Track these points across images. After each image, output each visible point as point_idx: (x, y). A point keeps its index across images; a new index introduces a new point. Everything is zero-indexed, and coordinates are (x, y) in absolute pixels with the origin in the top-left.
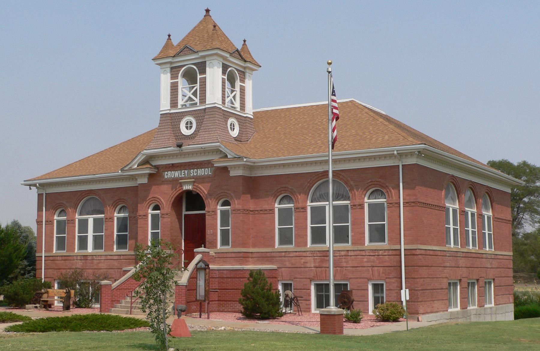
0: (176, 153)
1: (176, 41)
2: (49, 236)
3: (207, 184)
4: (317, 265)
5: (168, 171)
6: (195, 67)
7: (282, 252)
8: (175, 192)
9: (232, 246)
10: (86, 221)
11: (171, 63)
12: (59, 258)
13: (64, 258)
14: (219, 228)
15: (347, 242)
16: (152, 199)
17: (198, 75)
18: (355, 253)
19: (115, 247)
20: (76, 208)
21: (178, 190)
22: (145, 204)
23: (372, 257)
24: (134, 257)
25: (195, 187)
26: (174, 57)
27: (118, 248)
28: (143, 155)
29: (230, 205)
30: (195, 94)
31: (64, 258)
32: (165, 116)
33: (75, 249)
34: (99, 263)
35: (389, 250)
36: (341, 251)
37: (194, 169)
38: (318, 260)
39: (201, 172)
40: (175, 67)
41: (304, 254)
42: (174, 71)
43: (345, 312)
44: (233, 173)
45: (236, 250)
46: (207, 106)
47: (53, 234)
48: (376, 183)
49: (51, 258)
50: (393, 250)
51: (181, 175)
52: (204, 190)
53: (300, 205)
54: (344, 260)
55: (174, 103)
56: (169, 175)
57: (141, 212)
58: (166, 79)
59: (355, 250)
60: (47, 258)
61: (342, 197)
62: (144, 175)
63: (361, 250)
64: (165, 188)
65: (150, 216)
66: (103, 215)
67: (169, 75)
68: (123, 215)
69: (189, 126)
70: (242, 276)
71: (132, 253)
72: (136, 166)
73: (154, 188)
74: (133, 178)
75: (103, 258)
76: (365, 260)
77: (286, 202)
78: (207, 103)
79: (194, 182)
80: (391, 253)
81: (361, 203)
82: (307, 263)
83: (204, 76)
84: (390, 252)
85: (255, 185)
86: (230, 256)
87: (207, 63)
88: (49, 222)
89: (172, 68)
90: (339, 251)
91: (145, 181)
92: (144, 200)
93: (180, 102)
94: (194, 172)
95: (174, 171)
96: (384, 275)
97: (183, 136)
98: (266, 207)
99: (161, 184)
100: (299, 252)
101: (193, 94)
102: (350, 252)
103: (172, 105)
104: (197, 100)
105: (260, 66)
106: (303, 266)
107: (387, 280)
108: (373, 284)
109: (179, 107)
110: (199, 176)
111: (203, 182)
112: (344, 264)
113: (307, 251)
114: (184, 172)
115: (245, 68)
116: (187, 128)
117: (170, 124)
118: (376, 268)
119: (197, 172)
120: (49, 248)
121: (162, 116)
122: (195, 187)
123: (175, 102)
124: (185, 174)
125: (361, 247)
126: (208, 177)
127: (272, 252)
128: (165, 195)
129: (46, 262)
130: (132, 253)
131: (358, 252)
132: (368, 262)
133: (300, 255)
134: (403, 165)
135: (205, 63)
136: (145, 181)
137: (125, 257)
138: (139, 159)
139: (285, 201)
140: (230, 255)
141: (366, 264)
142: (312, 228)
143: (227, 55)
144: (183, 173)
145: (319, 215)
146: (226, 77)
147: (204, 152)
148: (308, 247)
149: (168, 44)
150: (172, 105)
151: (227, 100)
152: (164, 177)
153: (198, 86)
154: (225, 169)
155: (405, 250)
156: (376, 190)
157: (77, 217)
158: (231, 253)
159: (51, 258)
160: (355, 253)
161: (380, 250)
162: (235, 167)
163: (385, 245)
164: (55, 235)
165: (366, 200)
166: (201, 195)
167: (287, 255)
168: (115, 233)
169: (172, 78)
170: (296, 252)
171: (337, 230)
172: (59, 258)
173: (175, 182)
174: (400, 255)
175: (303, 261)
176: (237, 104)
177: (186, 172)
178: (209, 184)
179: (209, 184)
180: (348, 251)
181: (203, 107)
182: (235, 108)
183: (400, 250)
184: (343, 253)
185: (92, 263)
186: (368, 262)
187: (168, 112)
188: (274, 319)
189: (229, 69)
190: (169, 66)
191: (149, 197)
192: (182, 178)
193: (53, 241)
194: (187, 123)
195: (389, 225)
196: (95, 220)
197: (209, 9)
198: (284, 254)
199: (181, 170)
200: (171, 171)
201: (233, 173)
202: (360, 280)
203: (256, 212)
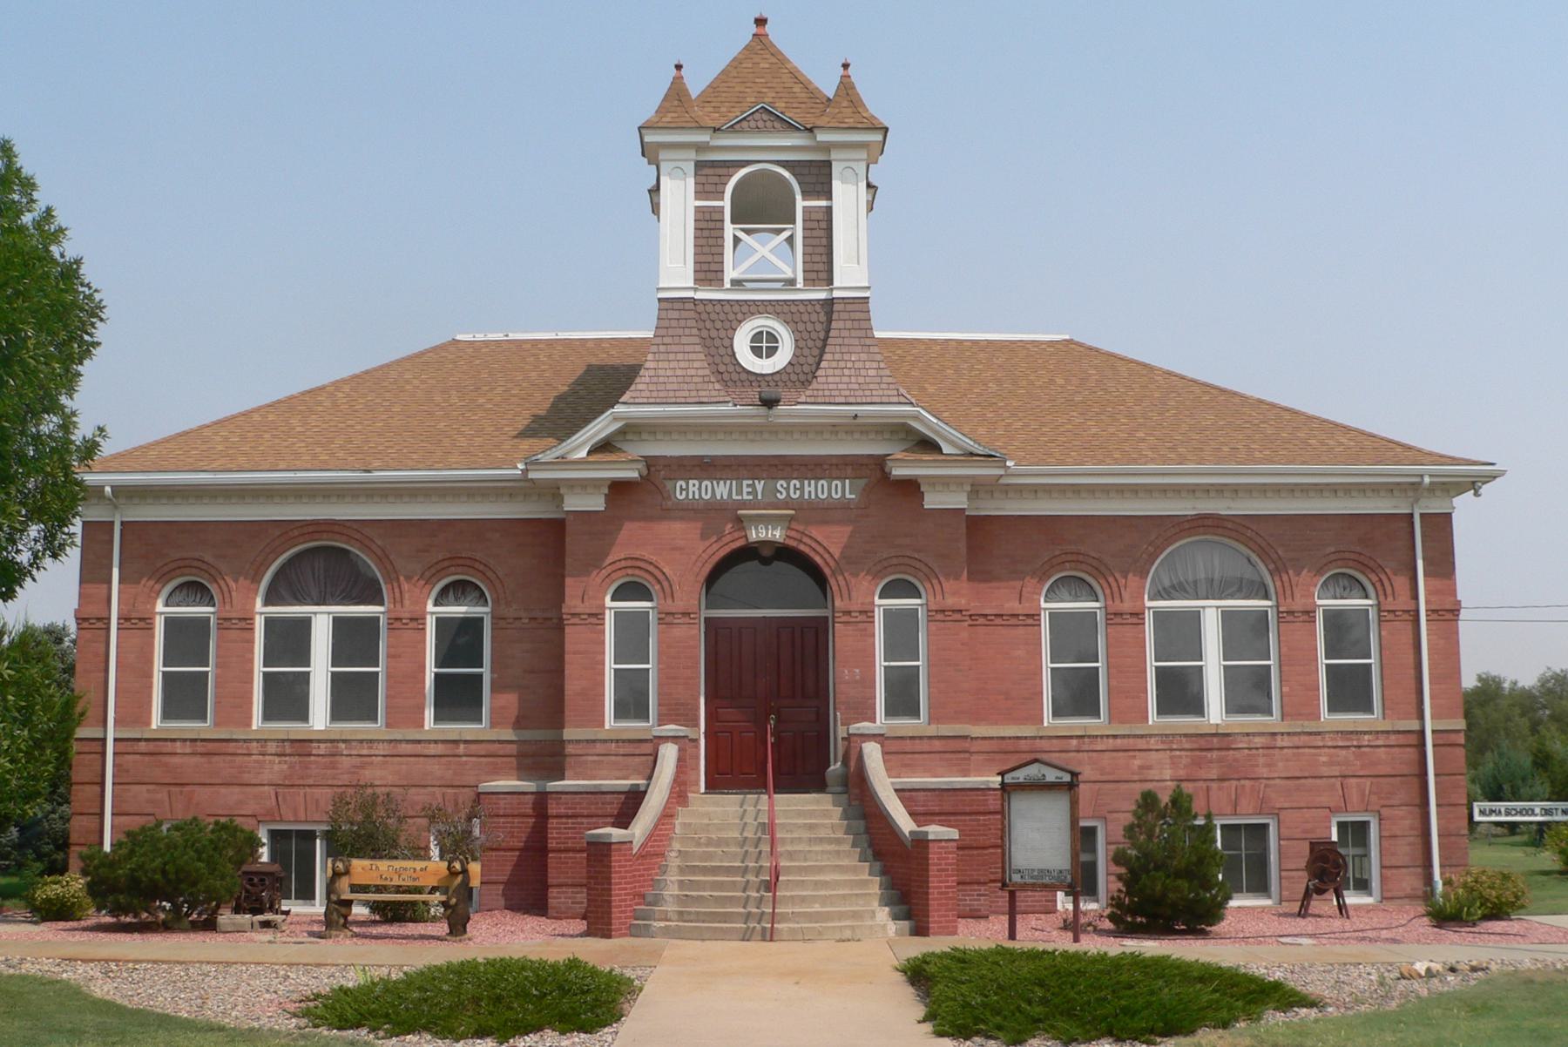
0: (757, 425)
1: (696, 85)
2: (137, 669)
3: (836, 528)
4: (1182, 773)
5: (687, 480)
6: (786, 174)
7: (1071, 737)
8: (715, 547)
9: (1111, 719)
10: (304, 625)
11: (700, 147)
12: (178, 747)
13: (200, 747)
14: (610, 666)
15: (373, 718)
16: (623, 564)
17: (799, 197)
18: (1296, 741)
19: (429, 713)
20: (256, 579)
21: (725, 540)
22: (596, 578)
23: (1344, 752)
24: (513, 749)
25: (793, 534)
26: (716, 130)
27: (438, 718)
28: (616, 419)
29: (651, 600)
31: (200, 747)
32: (677, 306)
33: (250, 718)
34: (362, 767)
35: (1388, 732)
36: (1254, 734)
37: (788, 479)
38: (1184, 761)
39: (816, 490)
40: (714, 164)
41: (1141, 744)
42: (709, 175)
44: (932, 501)
45: (947, 729)
46: (836, 294)
47: (150, 662)
48: (1347, 555)
49: (142, 746)
50: (1399, 732)
51: (740, 492)
52: (827, 543)
53: (1127, 606)
54: (1261, 760)
56: (690, 490)
57: (572, 603)
58: (680, 195)
59: (1295, 734)
60: (122, 747)
61: (1240, 589)
62: (594, 484)
63: (1310, 734)
64: (677, 531)
65: (879, 617)
67: (691, 181)
68: (463, 609)
69: (764, 345)
70: (982, 809)
71: (508, 734)
72: (583, 454)
73: (630, 529)
74: (554, 491)
75: (381, 749)
76: (1324, 759)
77: (1066, 594)
78: (836, 284)
79: (791, 518)
80: (1393, 739)
81: (867, 608)
82: (1150, 768)
83: (823, 203)
84: (1393, 737)
85: (995, 544)
86: (927, 748)
87: (836, 169)
88: (137, 622)
89: (699, 165)
90: (1248, 734)
91: (595, 503)
92: (594, 562)
94: (788, 489)
95: (710, 478)
96: (1374, 798)
97: (744, 377)
98: (1013, 606)
99: (661, 518)
100: (1124, 736)
102: (462, 746)
103: (702, 276)
106: (1136, 778)
107: (1385, 812)
109: (727, 285)
110: (809, 502)
111: (825, 522)
112: (1264, 772)
113: (1151, 736)
114: (753, 486)
117: (695, 331)
118: (1353, 781)
119: (802, 489)
120: (134, 711)
121: (665, 305)
122: (793, 534)
123: (714, 267)
124: (754, 492)
125: (1313, 723)
126: (844, 506)
127: (1034, 738)
128: (681, 554)
129: (121, 759)
130: (508, 734)
131: (1304, 738)
132: (1331, 764)
133: (1129, 747)
134: (122, 523)
136: (595, 503)
137: (473, 747)
138: (595, 434)
139: (1064, 592)
140: (925, 746)
141: (1325, 771)
142: (267, 677)
144: (745, 490)
145: (1181, 634)
147: (834, 429)
148: (154, 726)
149: (677, 92)
150: (702, 276)
152: (669, 496)
154: (911, 488)
155: (115, 740)
157: (261, 611)
158: (930, 738)
159: (142, 746)
160: (1296, 741)
161: (1365, 733)
162: (946, 482)
163: (1372, 719)
164: (158, 668)
165: (160, 607)
166: (818, 559)
167: (1086, 747)
168: (431, 670)
169: (700, 193)
170: (1115, 737)
171: (339, 684)
172: (178, 747)
173: (712, 515)
174: (104, 754)
175: (1137, 762)
177: (759, 486)
178: (850, 529)
179: (850, 529)
180: (1274, 734)
181: (822, 295)
183: (104, 740)
184: (1259, 741)
185: (333, 766)
186: (1331, 764)
187: (690, 294)
190: (692, 155)
191: (608, 561)
192: (744, 505)
193: (150, 687)
194: (757, 337)
195: (389, 676)
196: (339, 624)
197: (765, 15)
198: (1074, 742)
199: (739, 479)
200: (701, 479)
201: (932, 501)
202: (1308, 814)
203: (981, 621)
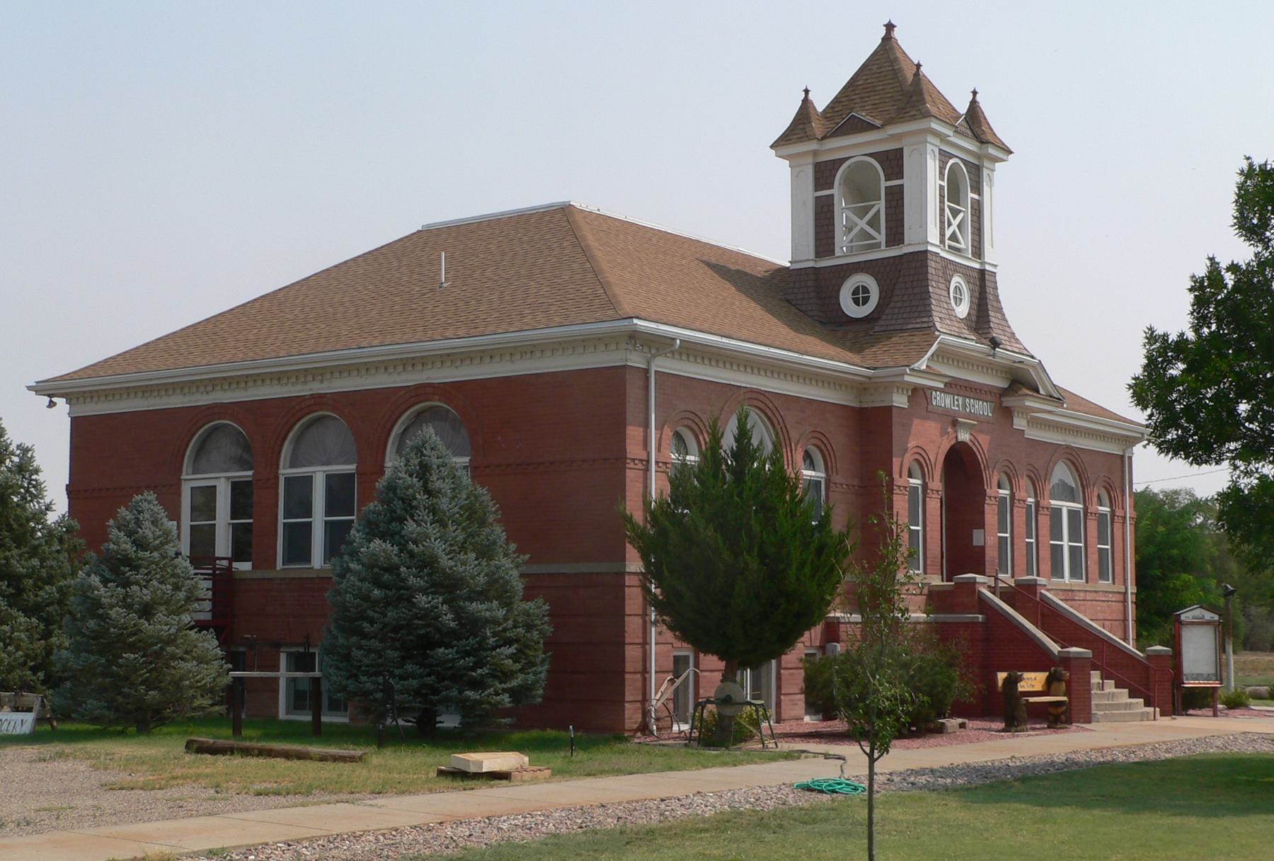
1: (821, 102)
11: (815, 153)
30: (873, 223)
43: (389, 721)
55: (824, 242)
66: (250, 473)
69: (860, 296)
93: (842, 242)
101: (870, 223)
104: (882, 238)
105: (1011, 153)
108: (289, 655)
115: (979, 157)
116: (856, 302)
135: (899, 153)
143: (948, 131)
146: (945, 184)
151: (948, 233)
153: (881, 205)
156: (419, 414)
169: (818, 187)
171: (211, 513)
176: (966, 243)
182: (959, 250)
188: (1069, 721)
189: (951, 162)
